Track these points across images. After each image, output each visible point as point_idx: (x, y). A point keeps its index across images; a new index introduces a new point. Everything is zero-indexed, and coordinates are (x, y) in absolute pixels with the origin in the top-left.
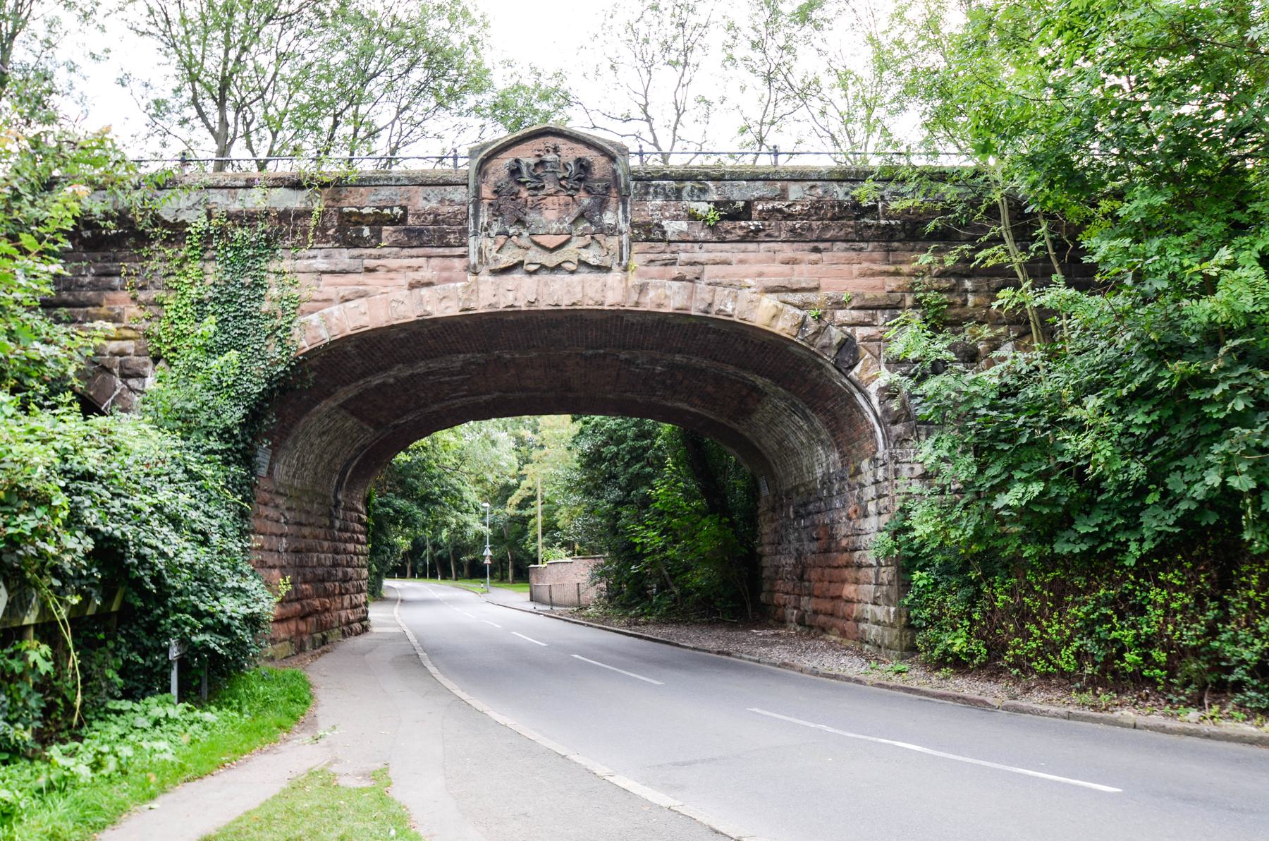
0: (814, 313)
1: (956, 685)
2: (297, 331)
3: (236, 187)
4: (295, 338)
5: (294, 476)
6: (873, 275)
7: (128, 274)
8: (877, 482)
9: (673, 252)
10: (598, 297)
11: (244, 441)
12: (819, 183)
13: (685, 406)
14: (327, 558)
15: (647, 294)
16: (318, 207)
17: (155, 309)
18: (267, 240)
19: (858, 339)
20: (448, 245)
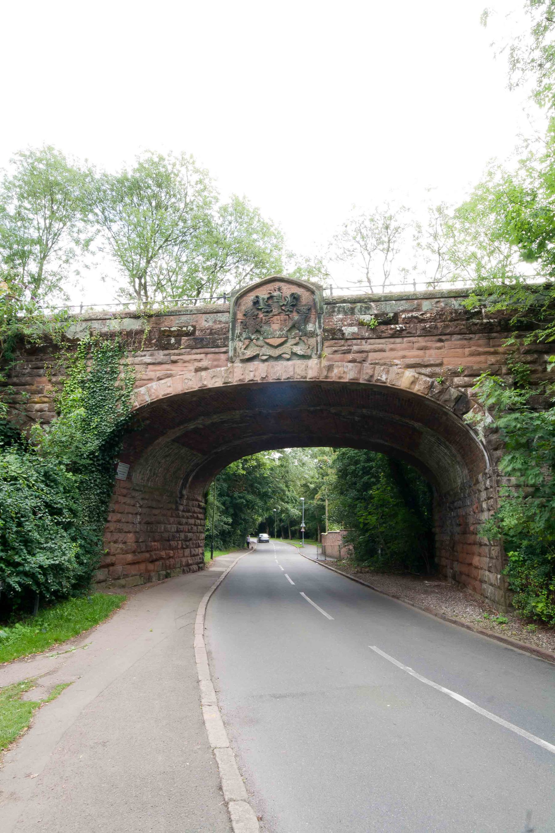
0: (438, 380)
1: (538, 639)
2: (133, 397)
3: (106, 319)
4: (132, 401)
5: (148, 480)
6: (479, 354)
7: (48, 368)
8: (486, 489)
9: (349, 346)
10: (303, 374)
11: (104, 460)
12: (442, 300)
13: (381, 441)
14: (174, 528)
15: (333, 371)
16: (147, 328)
17: (60, 386)
18: (119, 347)
19: (469, 396)
20: (218, 347)
